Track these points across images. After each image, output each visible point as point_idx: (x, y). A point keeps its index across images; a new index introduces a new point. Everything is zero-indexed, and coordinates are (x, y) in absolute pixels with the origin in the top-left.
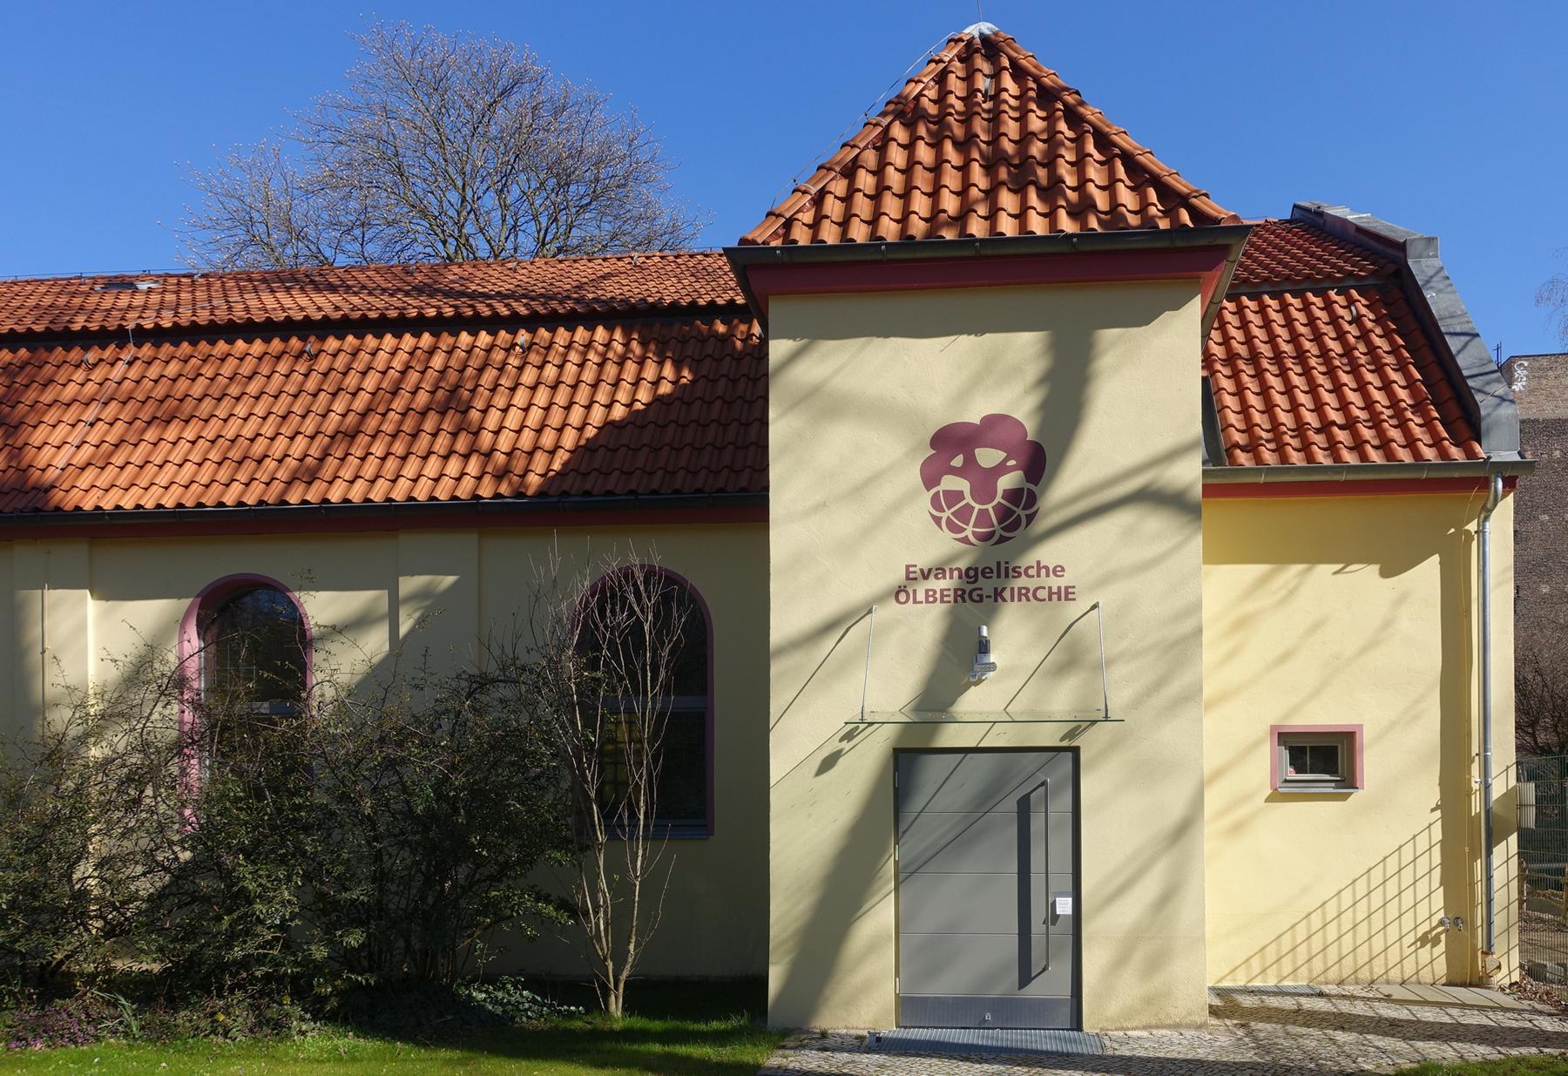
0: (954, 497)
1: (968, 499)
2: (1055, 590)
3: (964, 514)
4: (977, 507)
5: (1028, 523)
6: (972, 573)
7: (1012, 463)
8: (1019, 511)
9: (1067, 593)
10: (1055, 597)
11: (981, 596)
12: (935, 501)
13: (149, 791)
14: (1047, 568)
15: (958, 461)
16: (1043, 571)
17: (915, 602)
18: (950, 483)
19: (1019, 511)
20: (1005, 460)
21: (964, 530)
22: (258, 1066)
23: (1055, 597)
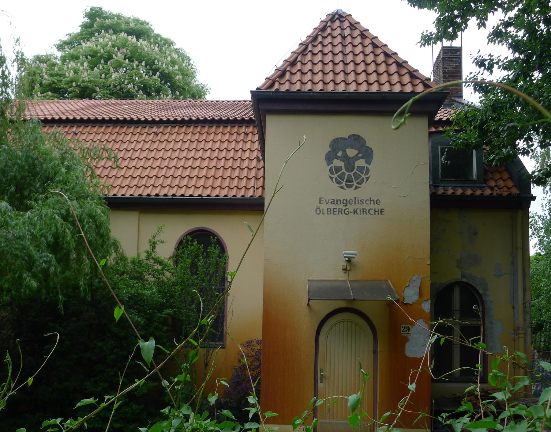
0: (338, 169)
1: (344, 170)
2: (377, 210)
3: (342, 177)
4: (352, 173)
5: (330, 177)
6: (345, 202)
7: (360, 155)
8: (336, 175)
9: (381, 212)
10: (377, 213)
11: (348, 212)
12: (331, 170)
13: (533, 16)
14: (374, 201)
15: (340, 154)
16: (372, 202)
17: (323, 214)
18: (337, 163)
19: (336, 175)
20: (357, 155)
21: (342, 183)
22: (344, 10)
23: (377, 213)
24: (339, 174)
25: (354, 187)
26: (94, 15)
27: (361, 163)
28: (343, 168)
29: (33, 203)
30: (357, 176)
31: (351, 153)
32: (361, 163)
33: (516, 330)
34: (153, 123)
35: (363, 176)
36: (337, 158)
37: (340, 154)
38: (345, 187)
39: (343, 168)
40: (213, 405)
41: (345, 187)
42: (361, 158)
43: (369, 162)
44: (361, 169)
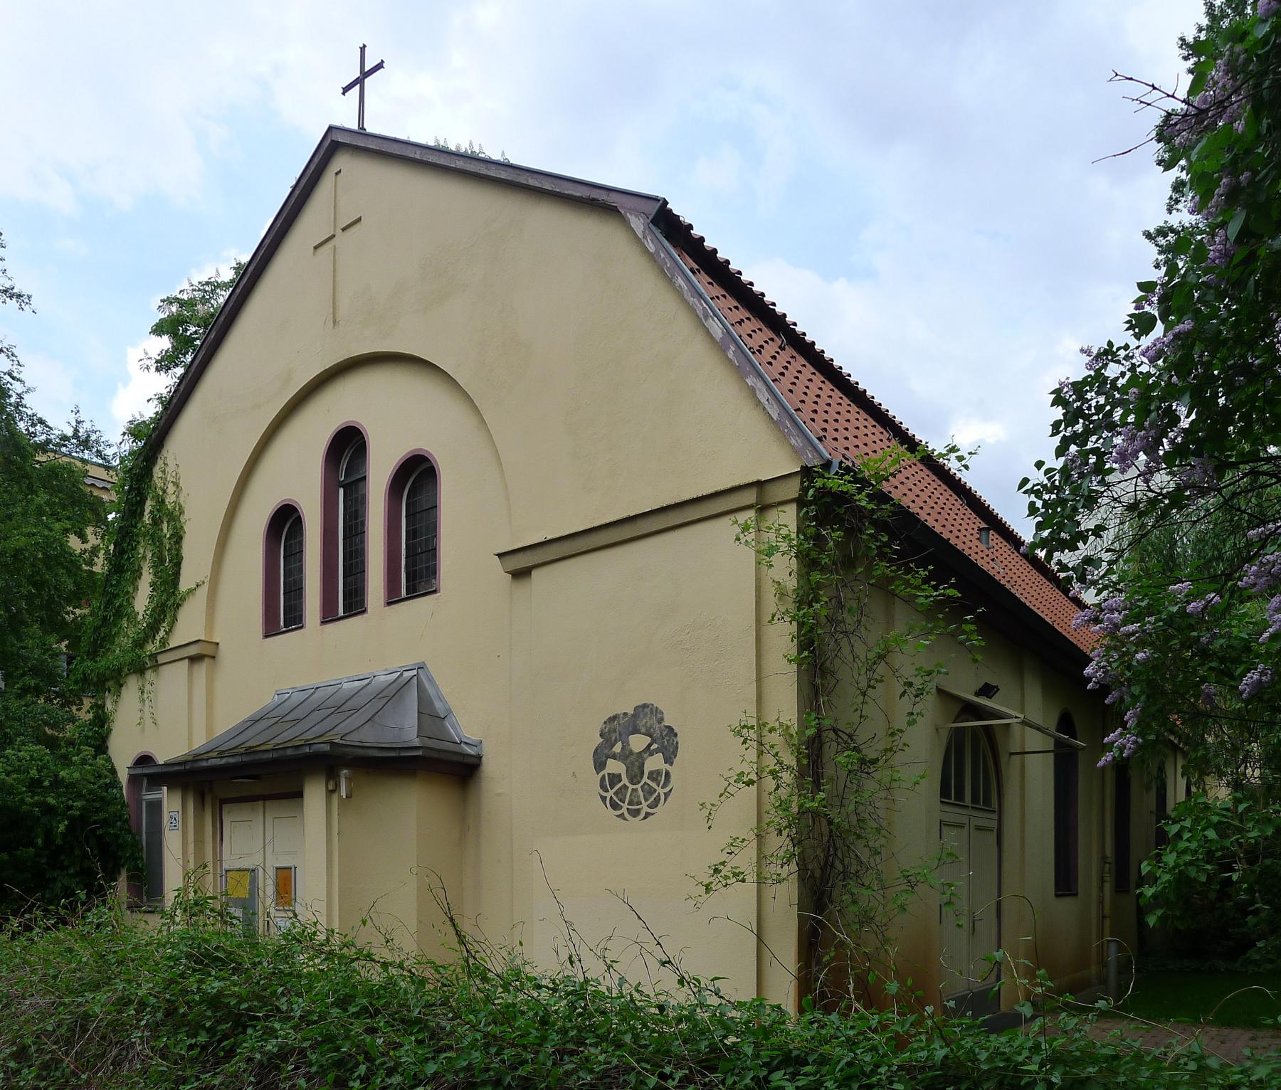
0: (615, 779)
1: (625, 781)
3: (621, 793)
7: (654, 746)
18: (614, 767)
19: (659, 790)
20: (650, 745)
24: (654, 785)
25: (619, 812)
26: (364, 612)
27: (655, 763)
28: (624, 777)
29: (1268, 862)
30: (649, 791)
31: (638, 743)
32: (655, 763)
33: (347, 961)
34: (759, 680)
35: (661, 791)
36: (614, 757)
37: (618, 748)
38: (627, 815)
39: (624, 777)
40: (112, 876)
41: (627, 815)
42: (657, 751)
43: (669, 760)
44: (654, 776)
